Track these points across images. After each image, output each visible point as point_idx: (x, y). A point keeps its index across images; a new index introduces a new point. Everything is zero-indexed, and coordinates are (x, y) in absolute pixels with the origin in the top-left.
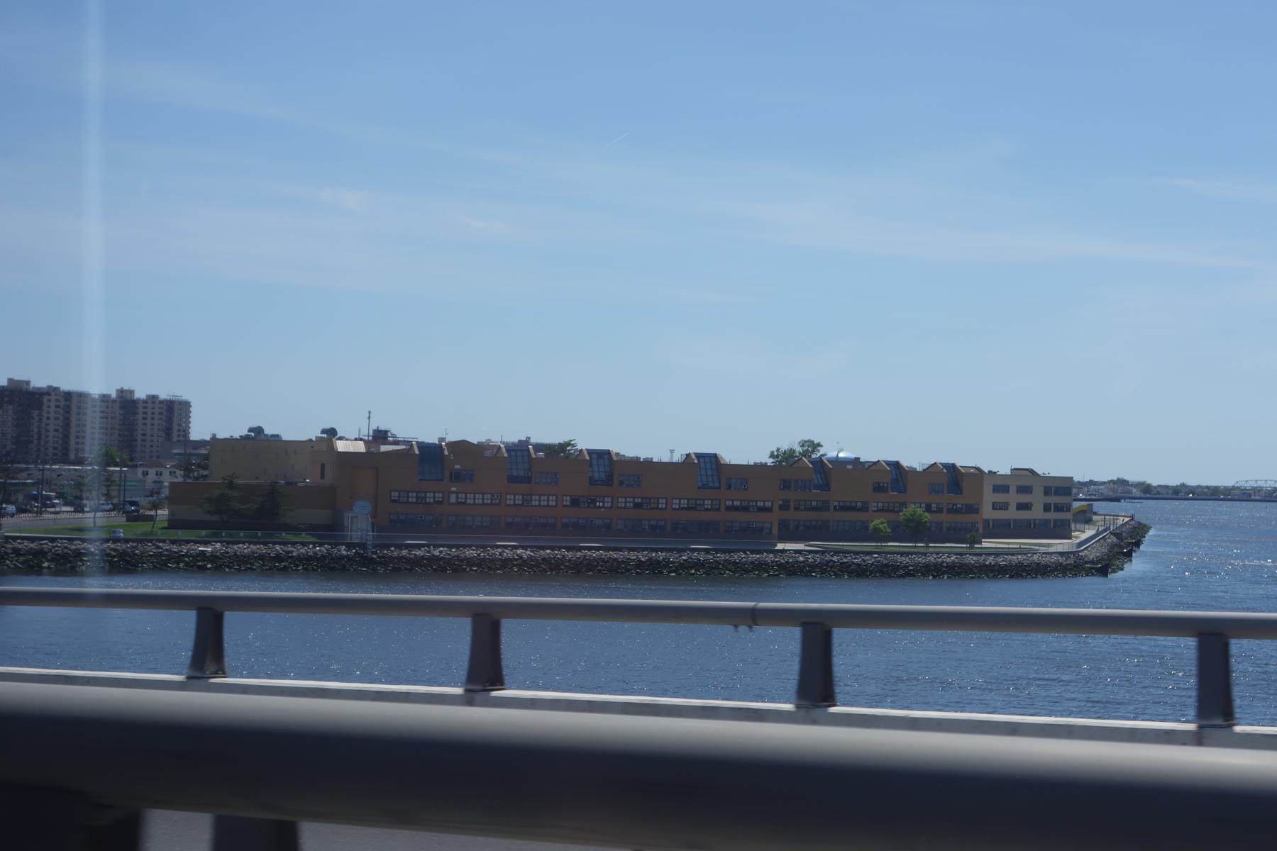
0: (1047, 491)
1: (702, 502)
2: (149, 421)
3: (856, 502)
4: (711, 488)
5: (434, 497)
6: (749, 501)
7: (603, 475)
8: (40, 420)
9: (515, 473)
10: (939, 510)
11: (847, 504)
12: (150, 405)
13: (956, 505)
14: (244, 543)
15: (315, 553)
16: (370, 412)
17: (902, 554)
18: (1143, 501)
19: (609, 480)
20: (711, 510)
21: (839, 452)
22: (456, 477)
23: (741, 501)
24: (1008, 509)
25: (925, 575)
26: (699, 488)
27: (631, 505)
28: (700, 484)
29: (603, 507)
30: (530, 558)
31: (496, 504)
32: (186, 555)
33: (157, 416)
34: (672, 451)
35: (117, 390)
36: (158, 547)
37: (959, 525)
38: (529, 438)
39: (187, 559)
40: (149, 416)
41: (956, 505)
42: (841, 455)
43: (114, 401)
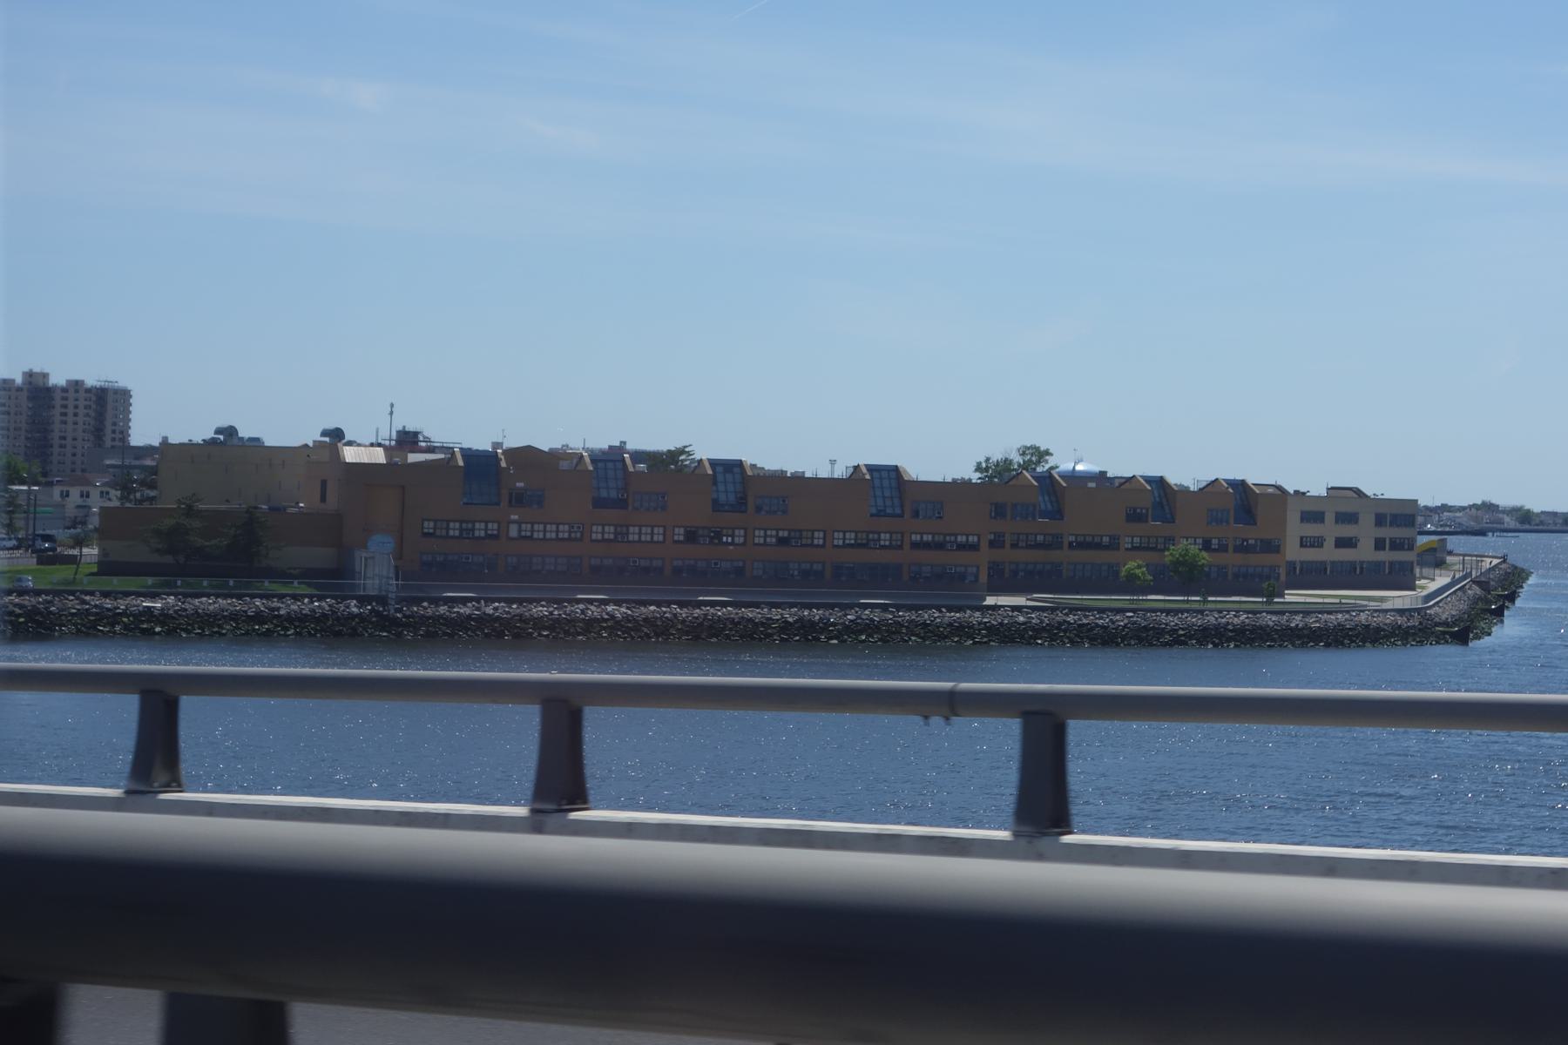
0: (1380, 520)
6: (945, 535)
7: (732, 498)
9: (604, 494)
10: (1223, 548)
11: (1089, 539)
12: (71, 395)
16: (392, 405)
17: (1168, 612)
19: (740, 504)
22: (518, 499)
26: (872, 515)
27: (774, 540)
28: (874, 511)
29: (732, 543)
30: (627, 618)
31: (576, 539)
32: (124, 614)
33: (81, 411)
36: (84, 602)
37: (1251, 570)
38: (625, 443)
40: (71, 411)
42: (1080, 467)
43: (19, 389)
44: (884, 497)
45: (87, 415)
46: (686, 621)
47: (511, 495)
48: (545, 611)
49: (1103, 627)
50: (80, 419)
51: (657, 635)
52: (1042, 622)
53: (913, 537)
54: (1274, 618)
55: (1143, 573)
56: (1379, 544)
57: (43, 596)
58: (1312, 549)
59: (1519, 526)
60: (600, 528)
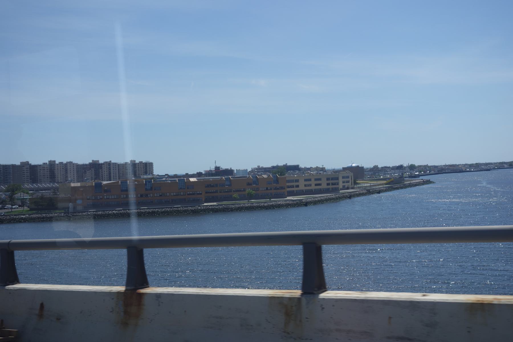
0: (328, 179)
1: (180, 193)
2: (140, 170)
3: (241, 189)
4: (183, 189)
5: (100, 197)
6: (195, 192)
7: (150, 188)
8: (102, 172)
9: (123, 189)
10: (271, 189)
11: (238, 190)
12: (140, 165)
13: (277, 187)
14: (35, 214)
15: (54, 216)
16: (215, 161)
17: (232, 205)
18: (499, 170)
19: (151, 189)
20: (183, 195)
21: (352, 164)
22: (106, 191)
23: (192, 192)
24: (311, 186)
25: (274, 208)
26: (179, 189)
27: (159, 195)
28: (179, 188)
29: (150, 197)
30: (117, 213)
31: (118, 198)
32: (17, 219)
33: (142, 168)
34: (323, 166)
35: (130, 161)
36: (10, 217)
37: (278, 193)
38: (287, 164)
39: (17, 220)
40: (140, 168)
41: (277, 187)
42: (354, 165)
43: (129, 164)
44: (182, 185)
45: (143, 169)
46: (155, 212)
47: (104, 190)
48: (100, 213)
49: (217, 209)
50: (142, 170)
51: (121, 216)
52: (204, 208)
53: (188, 193)
54: (256, 204)
55: (237, 197)
56: (316, 185)
57: (67, 214)
58: (308, 187)
59: (509, 167)
60: (111, 196)
